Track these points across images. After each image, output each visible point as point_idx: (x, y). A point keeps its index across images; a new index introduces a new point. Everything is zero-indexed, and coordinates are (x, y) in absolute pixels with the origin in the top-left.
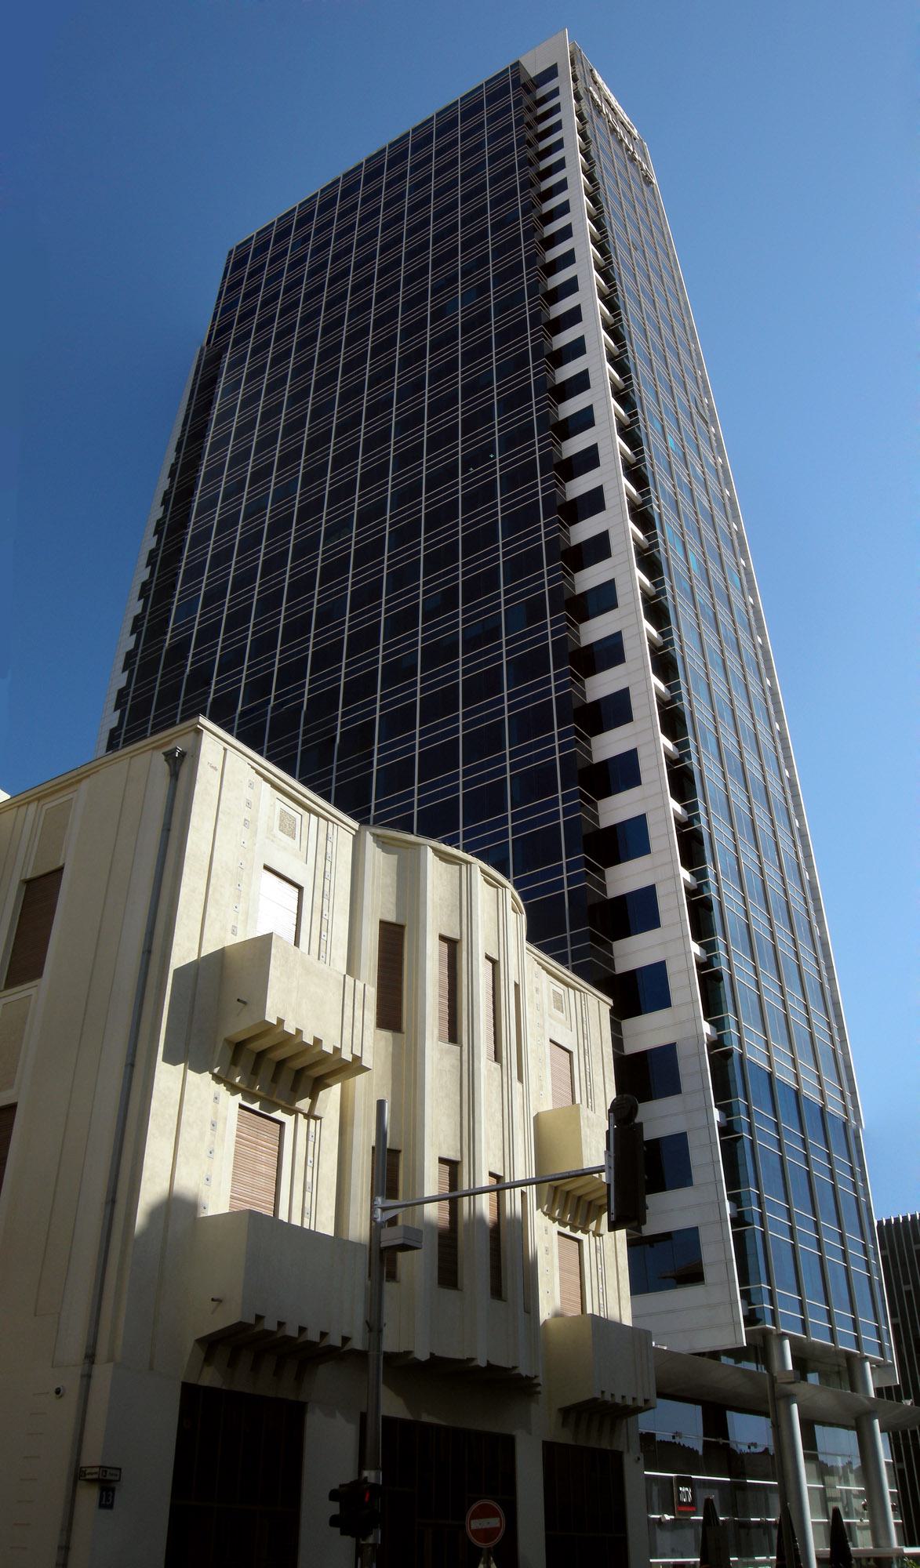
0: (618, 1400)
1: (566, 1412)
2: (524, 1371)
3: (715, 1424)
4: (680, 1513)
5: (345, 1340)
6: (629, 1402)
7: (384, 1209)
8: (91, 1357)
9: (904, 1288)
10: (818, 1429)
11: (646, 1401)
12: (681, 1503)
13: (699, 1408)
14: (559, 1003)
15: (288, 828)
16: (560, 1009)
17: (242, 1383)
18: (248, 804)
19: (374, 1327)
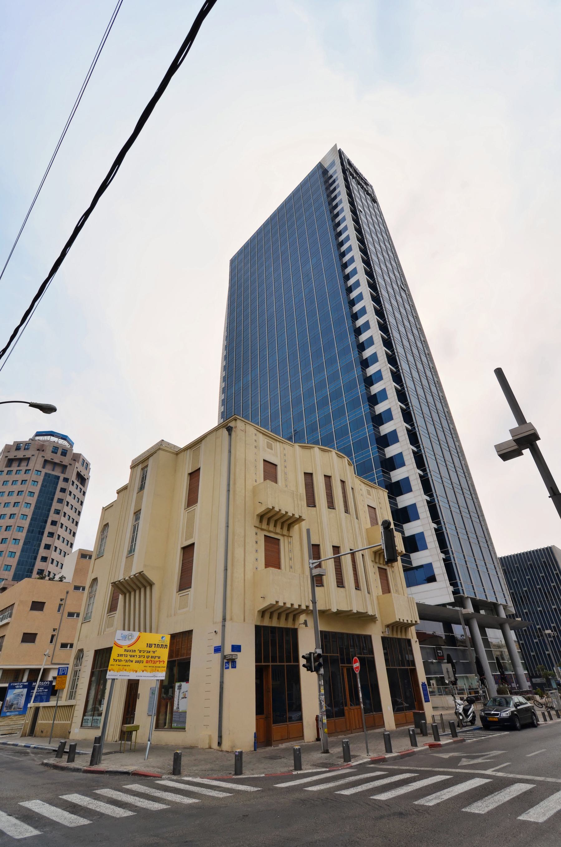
0: (405, 621)
1: (388, 626)
2: (370, 613)
3: (448, 628)
4: (439, 659)
5: (307, 607)
6: (410, 622)
7: (313, 563)
8: (224, 619)
9: (514, 580)
10: (487, 630)
11: (416, 621)
12: (438, 656)
13: (441, 624)
14: (369, 494)
15: (270, 447)
16: (370, 495)
17: (275, 623)
18: (255, 441)
19: (314, 602)
